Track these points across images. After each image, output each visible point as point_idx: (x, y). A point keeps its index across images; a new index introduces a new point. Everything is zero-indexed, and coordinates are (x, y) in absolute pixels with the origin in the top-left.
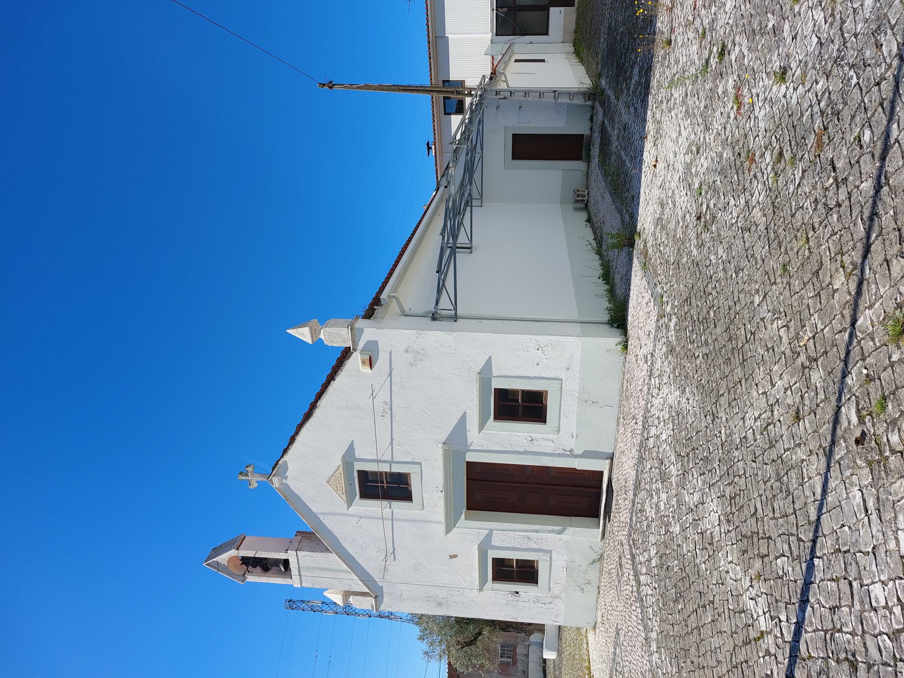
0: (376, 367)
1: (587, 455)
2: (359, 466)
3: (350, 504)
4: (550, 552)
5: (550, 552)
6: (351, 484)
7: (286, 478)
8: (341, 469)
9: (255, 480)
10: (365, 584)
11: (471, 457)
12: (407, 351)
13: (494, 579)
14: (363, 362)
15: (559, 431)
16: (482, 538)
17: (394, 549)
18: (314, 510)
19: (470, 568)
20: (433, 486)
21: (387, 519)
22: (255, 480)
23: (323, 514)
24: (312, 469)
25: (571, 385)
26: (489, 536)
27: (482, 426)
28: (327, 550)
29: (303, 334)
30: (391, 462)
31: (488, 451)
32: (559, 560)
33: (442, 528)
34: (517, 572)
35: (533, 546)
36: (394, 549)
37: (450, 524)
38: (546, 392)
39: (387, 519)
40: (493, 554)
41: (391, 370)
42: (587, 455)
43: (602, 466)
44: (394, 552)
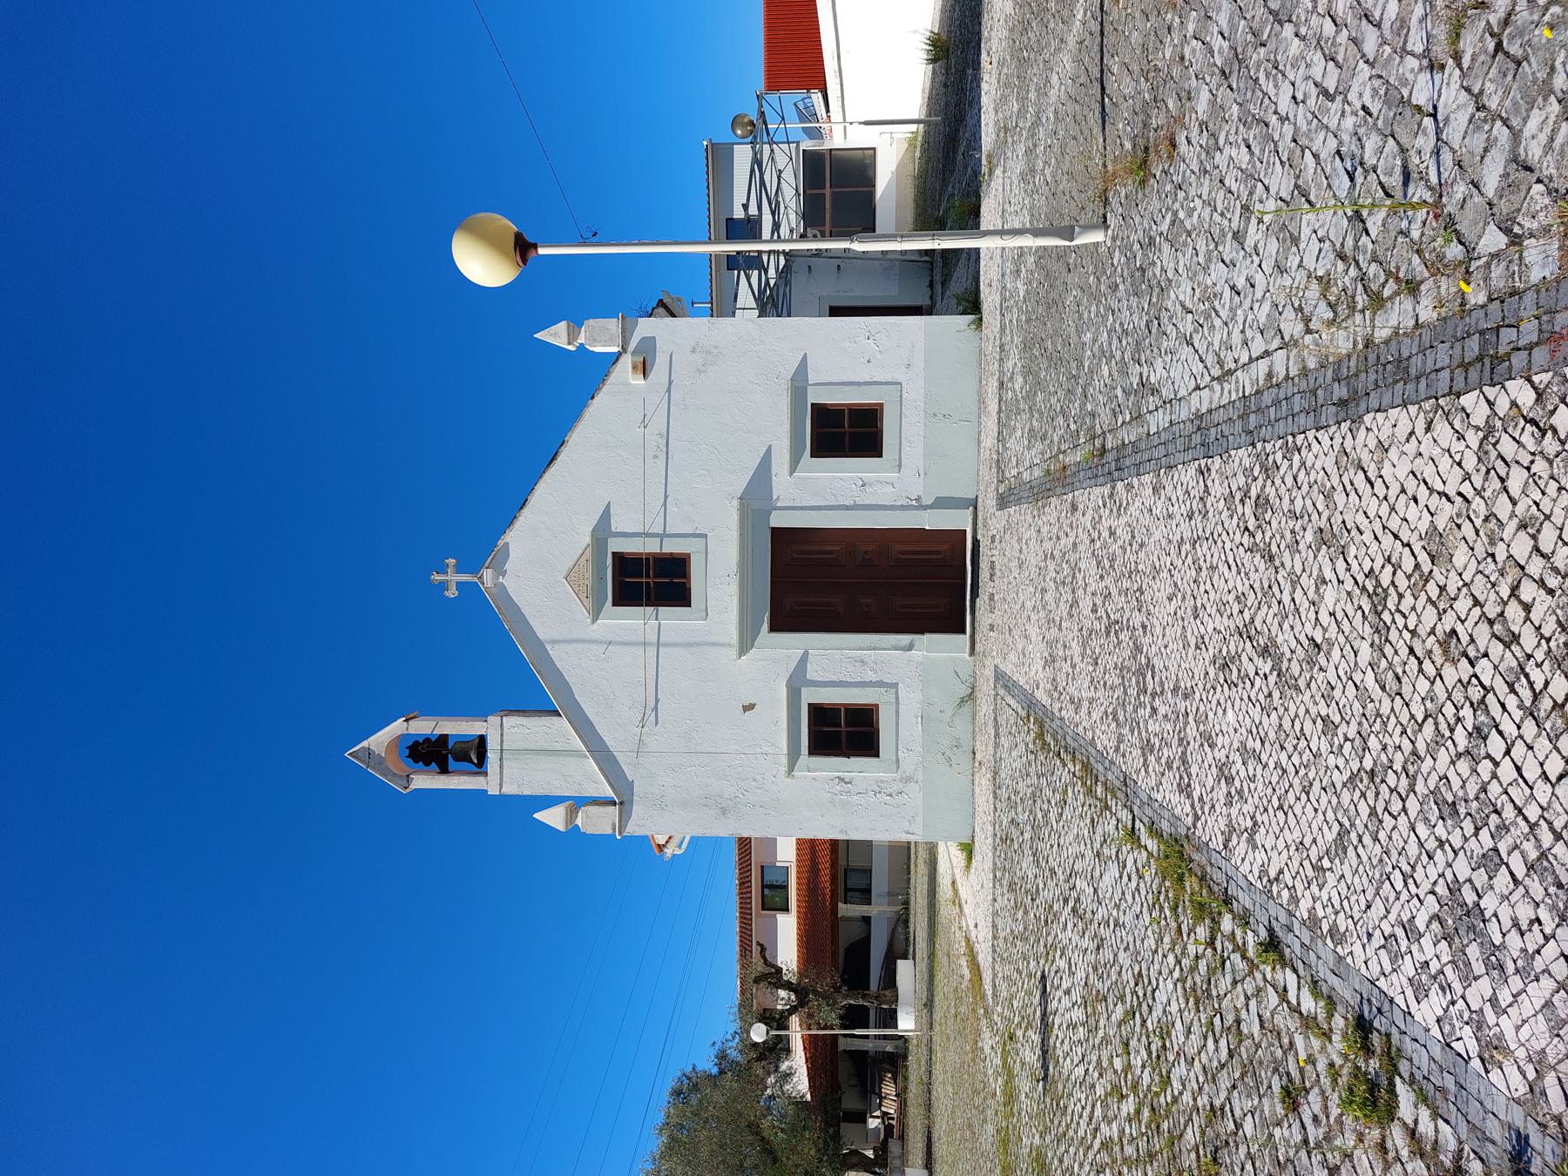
0: (651, 377)
1: (942, 503)
2: (617, 545)
3: (596, 615)
4: (895, 686)
5: (895, 686)
6: (603, 579)
7: (504, 574)
8: (590, 549)
9: (453, 579)
10: (611, 785)
11: (779, 520)
12: (693, 351)
13: (811, 753)
14: (635, 367)
15: (900, 466)
16: (792, 666)
17: (657, 701)
18: (541, 633)
19: (775, 728)
20: (723, 580)
21: (651, 644)
22: (453, 579)
23: (554, 642)
24: (539, 567)
25: (914, 393)
26: (804, 660)
27: (793, 469)
28: (556, 713)
29: (556, 335)
30: (662, 536)
31: (802, 508)
32: (911, 701)
33: (734, 652)
34: (843, 731)
35: (871, 676)
36: (657, 701)
37: (746, 643)
38: (877, 706)
39: (651, 644)
40: (811, 696)
41: (670, 383)
42: (942, 503)
43: (957, 520)
44: (656, 707)
